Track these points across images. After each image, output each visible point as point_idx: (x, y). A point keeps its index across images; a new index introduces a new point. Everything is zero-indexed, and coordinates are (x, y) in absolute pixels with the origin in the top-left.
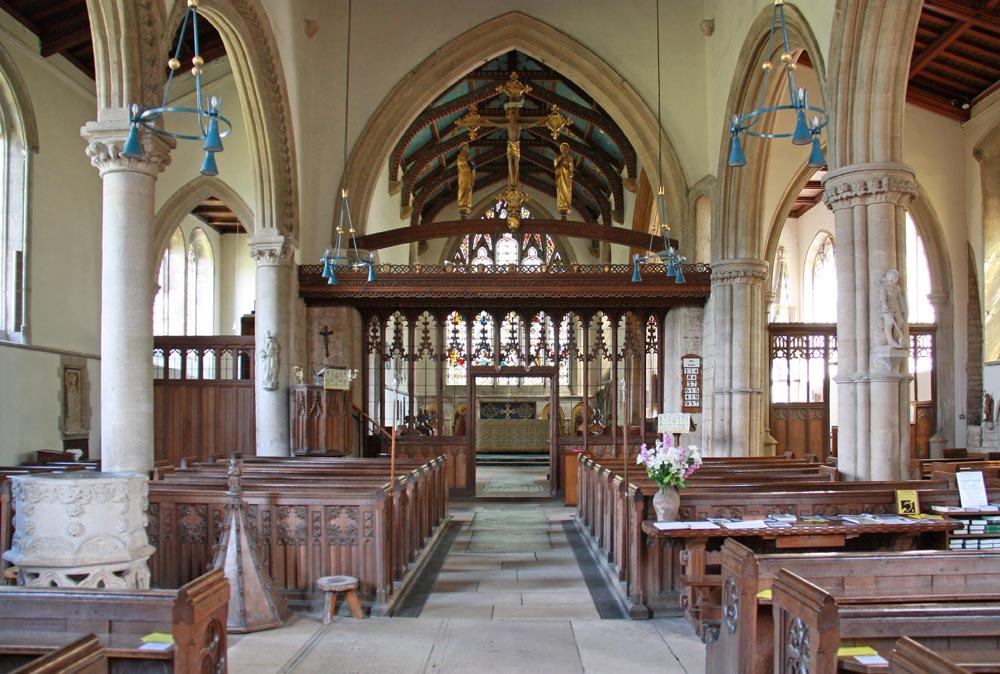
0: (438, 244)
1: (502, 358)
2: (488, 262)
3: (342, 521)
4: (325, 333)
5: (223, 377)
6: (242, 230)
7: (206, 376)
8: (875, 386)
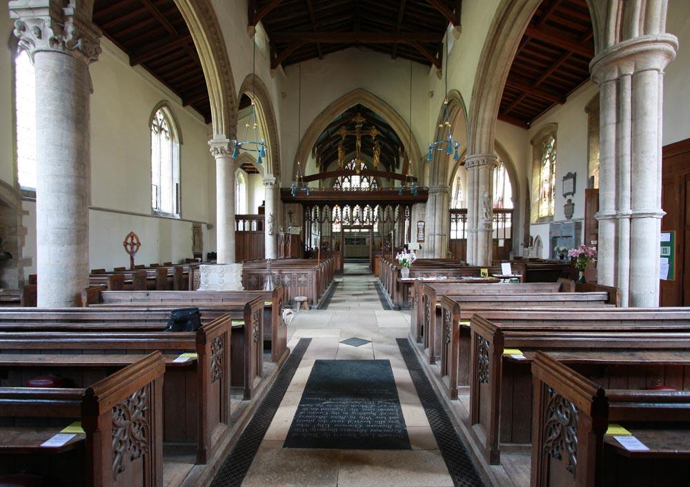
0: (329, 180)
1: (353, 222)
2: (349, 186)
3: (302, 279)
4: (290, 213)
5: (239, 230)
6: (258, 172)
7: (246, 230)
8: (479, 233)
